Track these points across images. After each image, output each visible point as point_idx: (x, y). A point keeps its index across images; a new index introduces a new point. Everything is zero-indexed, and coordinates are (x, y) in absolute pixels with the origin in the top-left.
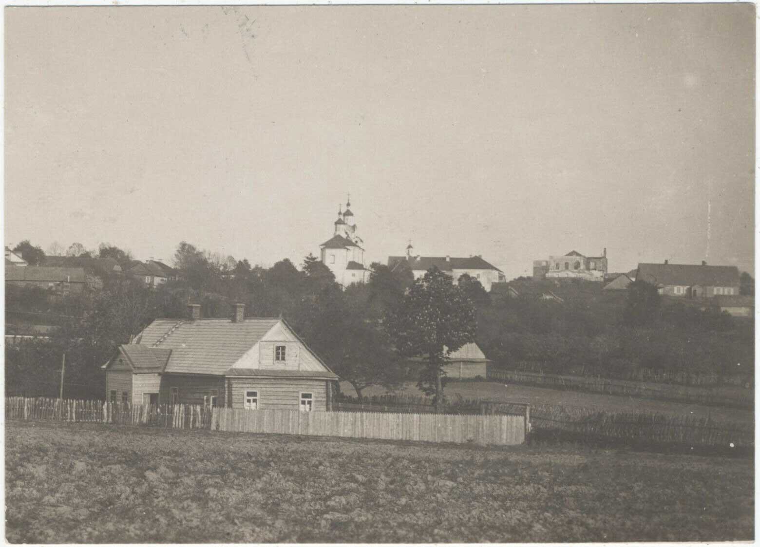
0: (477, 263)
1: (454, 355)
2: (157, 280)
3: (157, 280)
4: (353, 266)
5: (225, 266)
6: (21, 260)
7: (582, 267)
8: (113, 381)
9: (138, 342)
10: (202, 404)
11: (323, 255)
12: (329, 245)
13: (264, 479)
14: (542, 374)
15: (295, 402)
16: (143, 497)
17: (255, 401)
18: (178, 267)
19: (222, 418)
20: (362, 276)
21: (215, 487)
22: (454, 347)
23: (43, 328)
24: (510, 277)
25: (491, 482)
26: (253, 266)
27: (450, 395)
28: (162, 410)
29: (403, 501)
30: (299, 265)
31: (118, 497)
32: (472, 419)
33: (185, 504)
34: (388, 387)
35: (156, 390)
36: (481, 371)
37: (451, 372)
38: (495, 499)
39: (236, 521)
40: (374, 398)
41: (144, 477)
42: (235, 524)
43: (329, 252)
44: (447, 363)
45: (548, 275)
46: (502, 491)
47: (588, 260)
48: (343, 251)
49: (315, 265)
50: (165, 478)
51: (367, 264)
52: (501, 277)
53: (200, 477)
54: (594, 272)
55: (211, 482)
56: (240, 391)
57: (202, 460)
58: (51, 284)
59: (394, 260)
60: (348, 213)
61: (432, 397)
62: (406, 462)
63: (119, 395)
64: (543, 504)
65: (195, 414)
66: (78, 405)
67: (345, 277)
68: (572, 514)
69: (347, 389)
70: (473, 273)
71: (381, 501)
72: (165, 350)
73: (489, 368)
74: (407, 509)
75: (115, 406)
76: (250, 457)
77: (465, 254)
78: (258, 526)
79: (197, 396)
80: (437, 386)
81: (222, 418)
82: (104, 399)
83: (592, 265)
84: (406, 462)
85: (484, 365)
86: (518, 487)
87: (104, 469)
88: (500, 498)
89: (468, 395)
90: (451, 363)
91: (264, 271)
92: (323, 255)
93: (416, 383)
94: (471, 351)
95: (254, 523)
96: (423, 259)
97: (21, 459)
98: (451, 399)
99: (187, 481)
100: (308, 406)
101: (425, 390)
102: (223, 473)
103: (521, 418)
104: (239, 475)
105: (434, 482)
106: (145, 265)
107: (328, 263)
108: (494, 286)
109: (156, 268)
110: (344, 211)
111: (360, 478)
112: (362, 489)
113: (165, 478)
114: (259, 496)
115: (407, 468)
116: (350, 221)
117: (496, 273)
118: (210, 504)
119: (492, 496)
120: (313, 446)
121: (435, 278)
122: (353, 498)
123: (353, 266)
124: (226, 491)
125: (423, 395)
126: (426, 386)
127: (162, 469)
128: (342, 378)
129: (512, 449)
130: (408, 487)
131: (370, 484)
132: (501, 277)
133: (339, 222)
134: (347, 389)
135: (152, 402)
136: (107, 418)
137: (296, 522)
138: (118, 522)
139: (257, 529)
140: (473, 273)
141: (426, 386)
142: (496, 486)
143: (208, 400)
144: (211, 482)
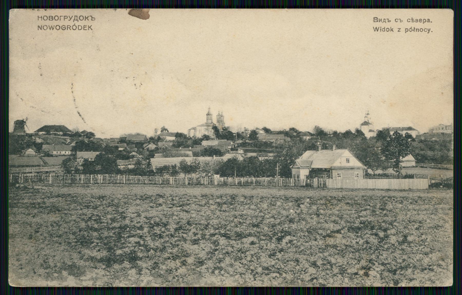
0: (410, 129)
1: (404, 159)
2: (308, 138)
3: (308, 138)
4: (370, 131)
5: (330, 132)
6: (264, 133)
7: (444, 128)
8: (294, 171)
9: (302, 159)
10: (323, 178)
11: (361, 128)
12: (362, 124)
13: (339, 206)
14: (433, 164)
15: (353, 176)
16: (299, 214)
17: (340, 176)
18: (314, 133)
19: (330, 183)
20: (374, 134)
21: (323, 209)
22: (403, 157)
23: (271, 154)
24: (422, 132)
25: (414, 204)
26: (338, 132)
27: (404, 172)
28: (310, 180)
29: (385, 212)
30: (353, 131)
31: (290, 215)
32: (411, 180)
33: (312, 216)
34: (383, 171)
35: (308, 174)
36: (414, 164)
37: (403, 164)
38: (415, 210)
39: (328, 222)
40: (379, 174)
41: (300, 207)
42: (328, 223)
43: (363, 126)
44: (402, 162)
45: (434, 132)
46: (417, 208)
47: (446, 127)
48: (367, 126)
49: (359, 132)
50: (306, 207)
51: (375, 130)
52: (418, 133)
53: (318, 206)
54: (448, 130)
55: (322, 208)
56: (335, 173)
57: (319, 200)
58: (274, 140)
59: (384, 129)
60: (368, 114)
61: (398, 173)
62: (387, 198)
63: (296, 176)
64: (431, 212)
65: (321, 181)
66: (283, 180)
67: (368, 135)
68: (440, 215)
69: (370, 171)
70: (409, 132)
71: (377, 213)
72: (310, 161)
73: (416, 162)
74: (386, 215)
75: (295, 180)
76: (335, 198)
77: (406, 126)
78: (336, 224)
79: (321, 175)
80: (399, 169)
81: (330, 183)
82: (291, 177)
83: (447, 128)
84: (387, 198)
85: (414, 162)
86: (423, 206)
87: (287, 204)
88: (417, 210)
89: (410, 172)
90: (403, 162)
91: (342, 133)
92: (361, 128)
93: (392, 168)
94: (410, 157)
95: (334, 223)
96: (393, 128)
97: (260, 201)
98: (404, 174)
99: (314, 207)
100: (357, 178)
101: (395, 171)
102: (326, 204)
103: (427, 179)
104: (331, 205)
105: (395, 205)
106: (304, 133)
107: (362, 130)
108: (417, 136)
109: (306, 134)
110: (367, 113)
111: (371, 205)
112: (371, 209)
113: (306, 207)
114: (337, 212)
115: (387, 200)
116: (369, 116)
117: (417, 132)
118: (321, 216)
119: (414, 210)
120: (354, 193)
121: (396, 134)
122: (368, 212)
123: (370, 131)
124: (326, 211)
125: (395, 172)
126: (396, 170)
127: (306, 204)
128: (368, 168)
129: (424, 191)
130: (386, 207)
131: (374, 207)
132: (418, 133)
133: (366, 117)
134: (370, 171)
135: (307, 178)
136: (292, 184)
137: (348, 222)
138: (289, 224)
139: (335, 225)
140: (409, 132)
141: (396, 170)
142: (416, 206)
143: (325, 177)
144: (322, 208)
